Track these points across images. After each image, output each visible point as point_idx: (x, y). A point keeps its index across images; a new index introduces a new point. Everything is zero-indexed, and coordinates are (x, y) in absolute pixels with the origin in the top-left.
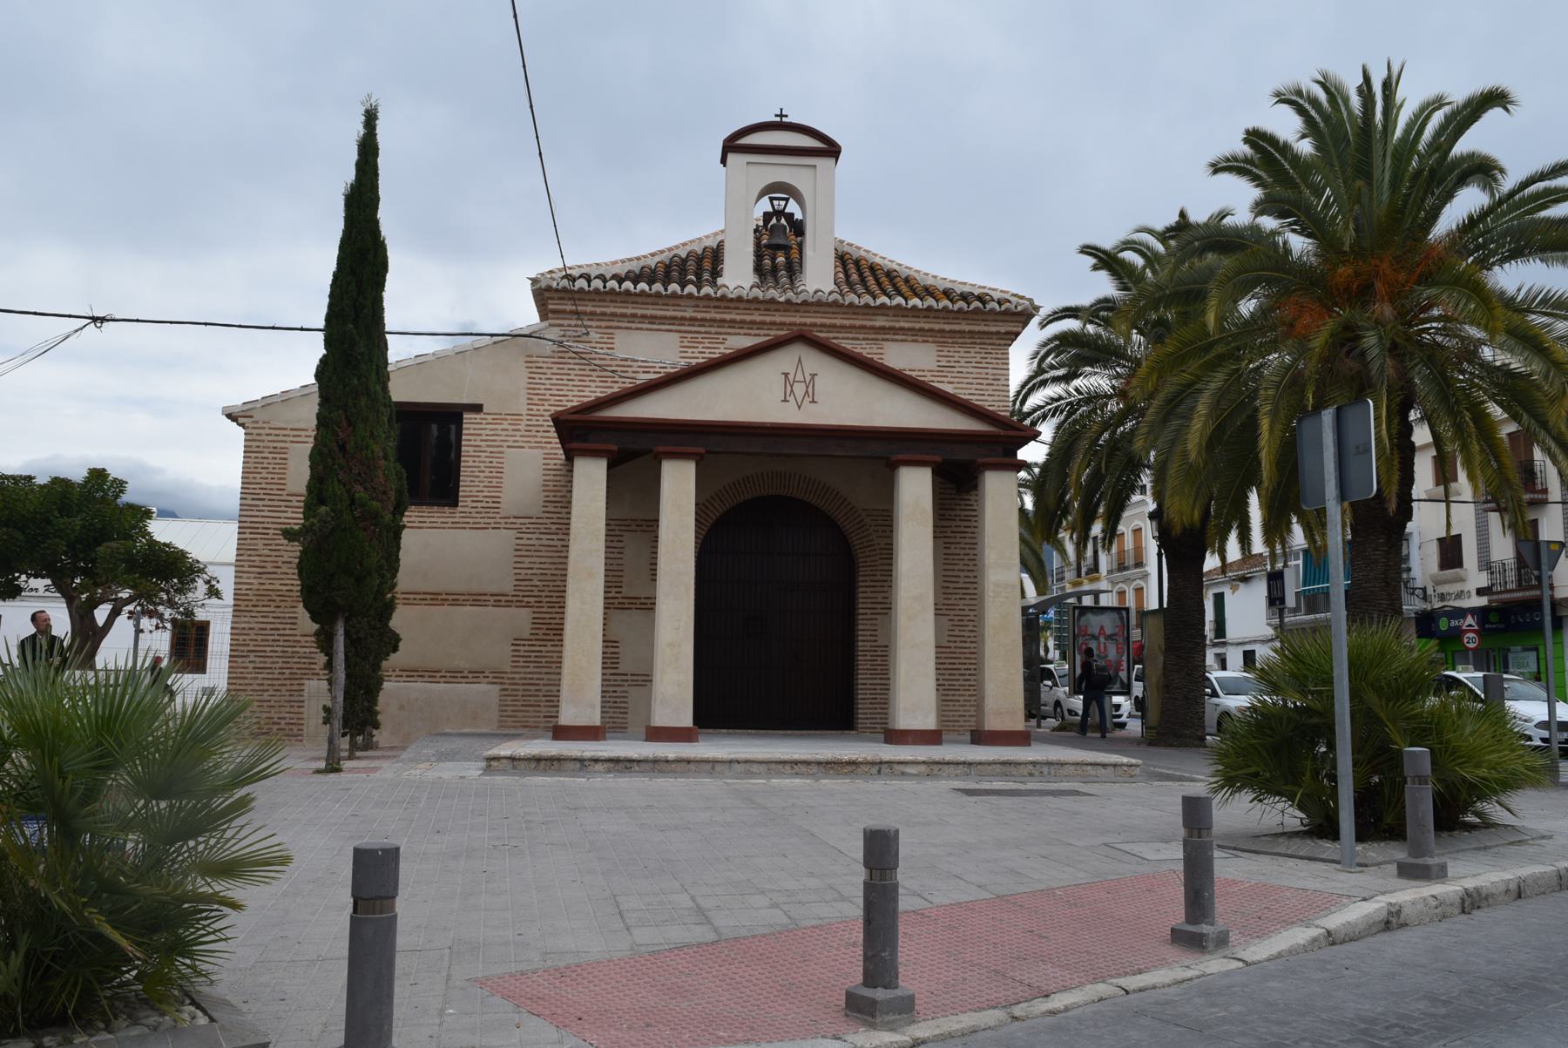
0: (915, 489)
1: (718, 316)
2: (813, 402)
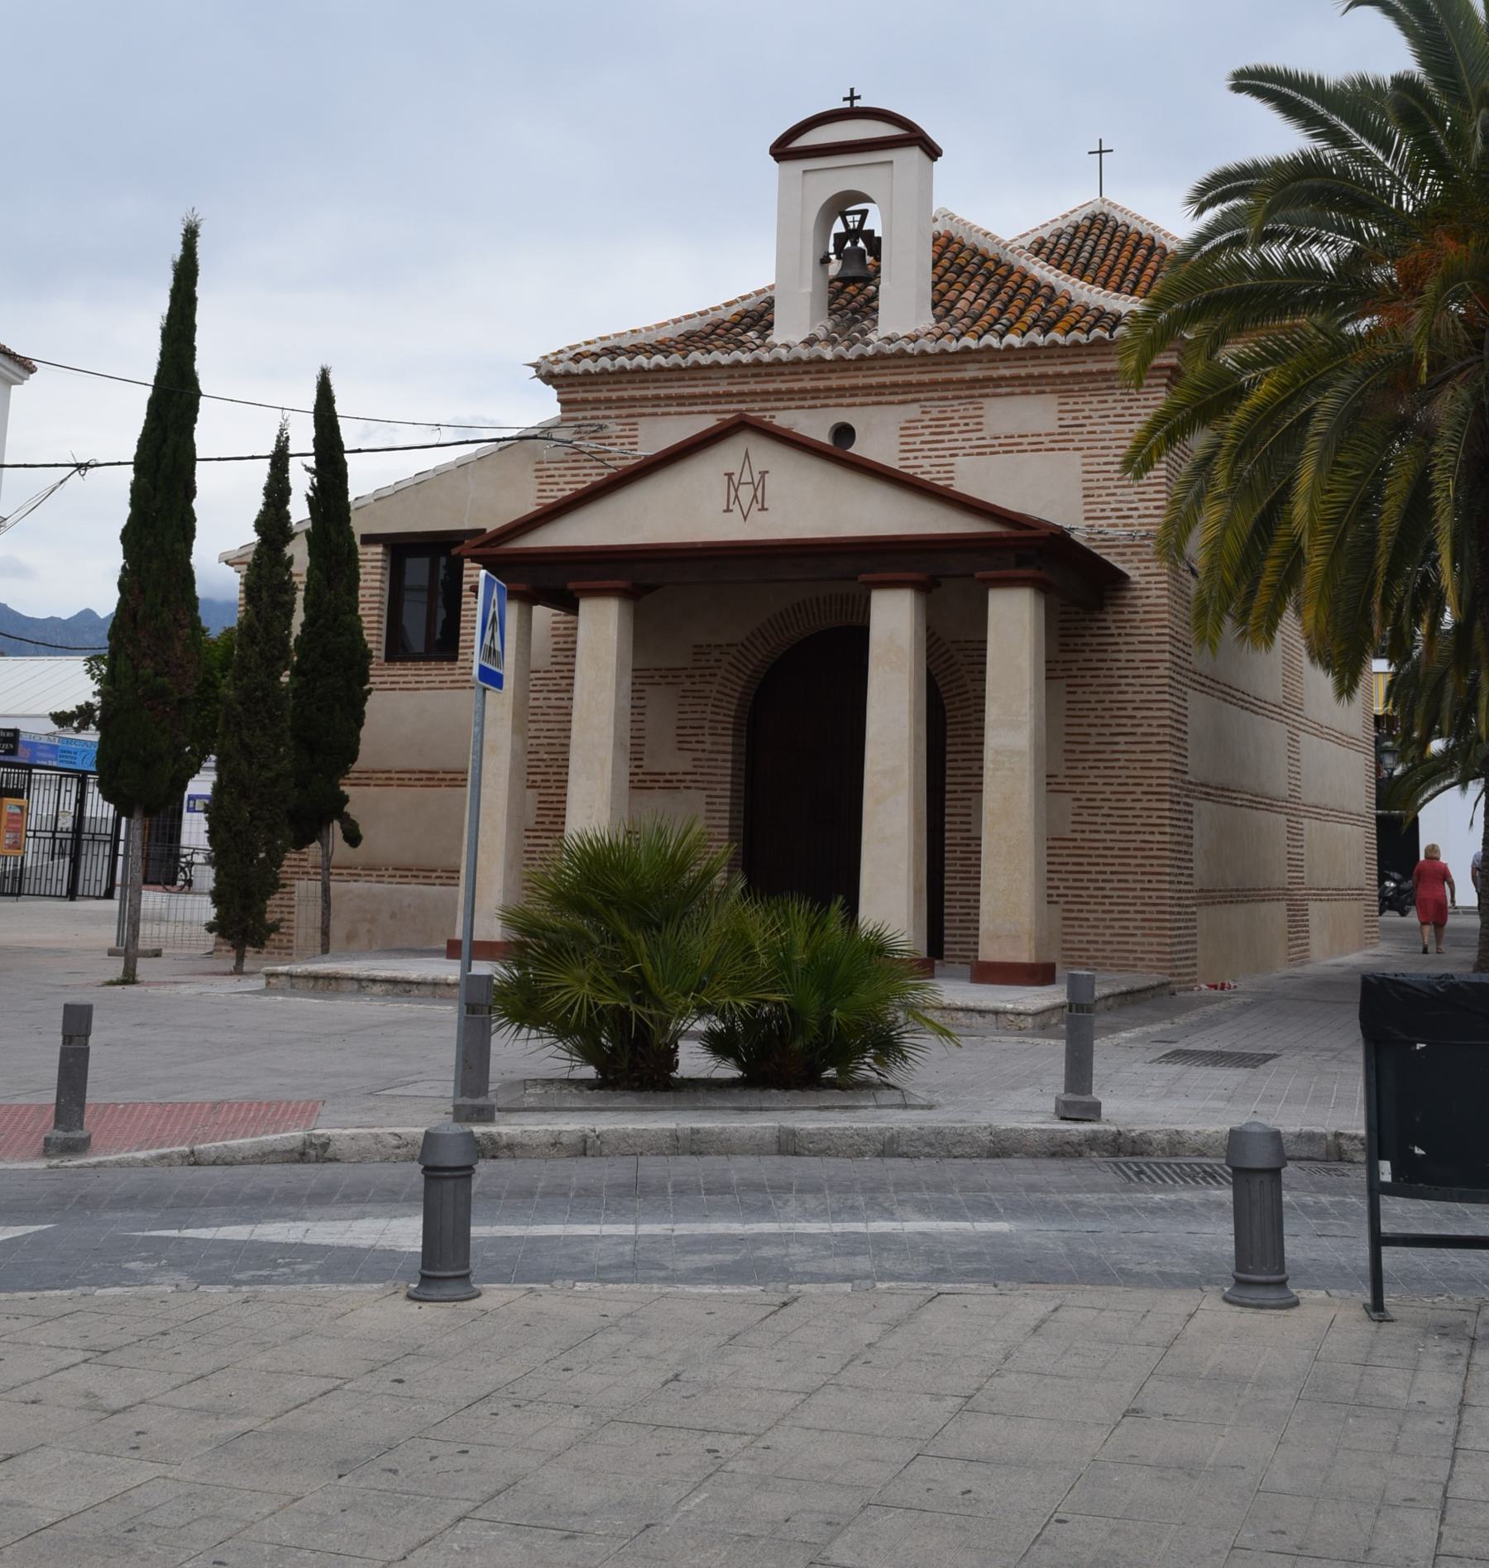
0: (894, 621)
1: (759, 388)
2: (763, 509)
